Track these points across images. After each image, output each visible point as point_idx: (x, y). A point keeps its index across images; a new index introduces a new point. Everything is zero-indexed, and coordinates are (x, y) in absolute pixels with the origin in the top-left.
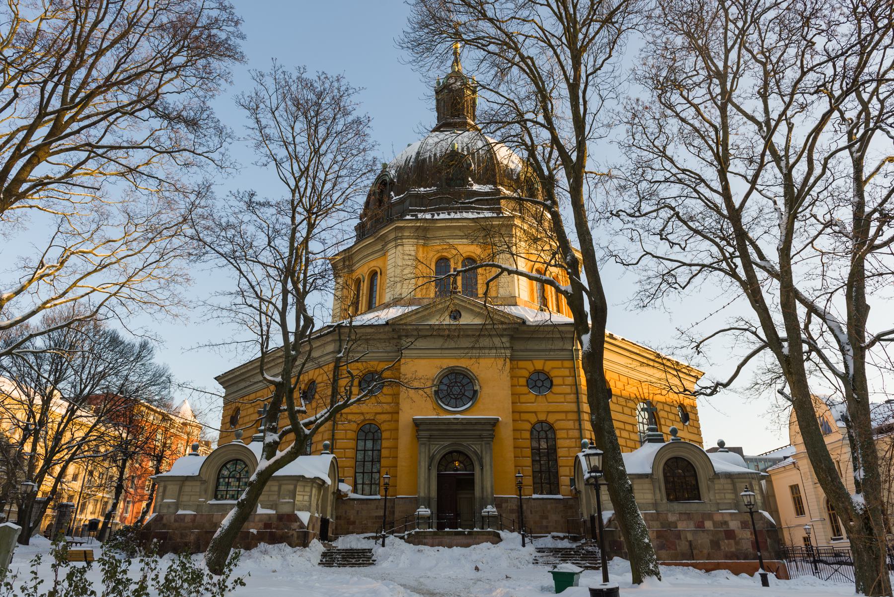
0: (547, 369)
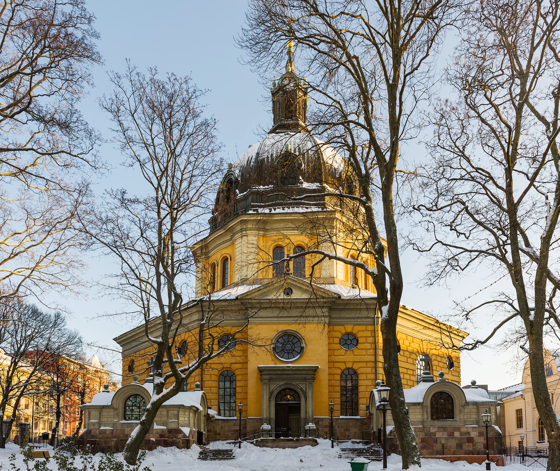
0: (354, 332)
